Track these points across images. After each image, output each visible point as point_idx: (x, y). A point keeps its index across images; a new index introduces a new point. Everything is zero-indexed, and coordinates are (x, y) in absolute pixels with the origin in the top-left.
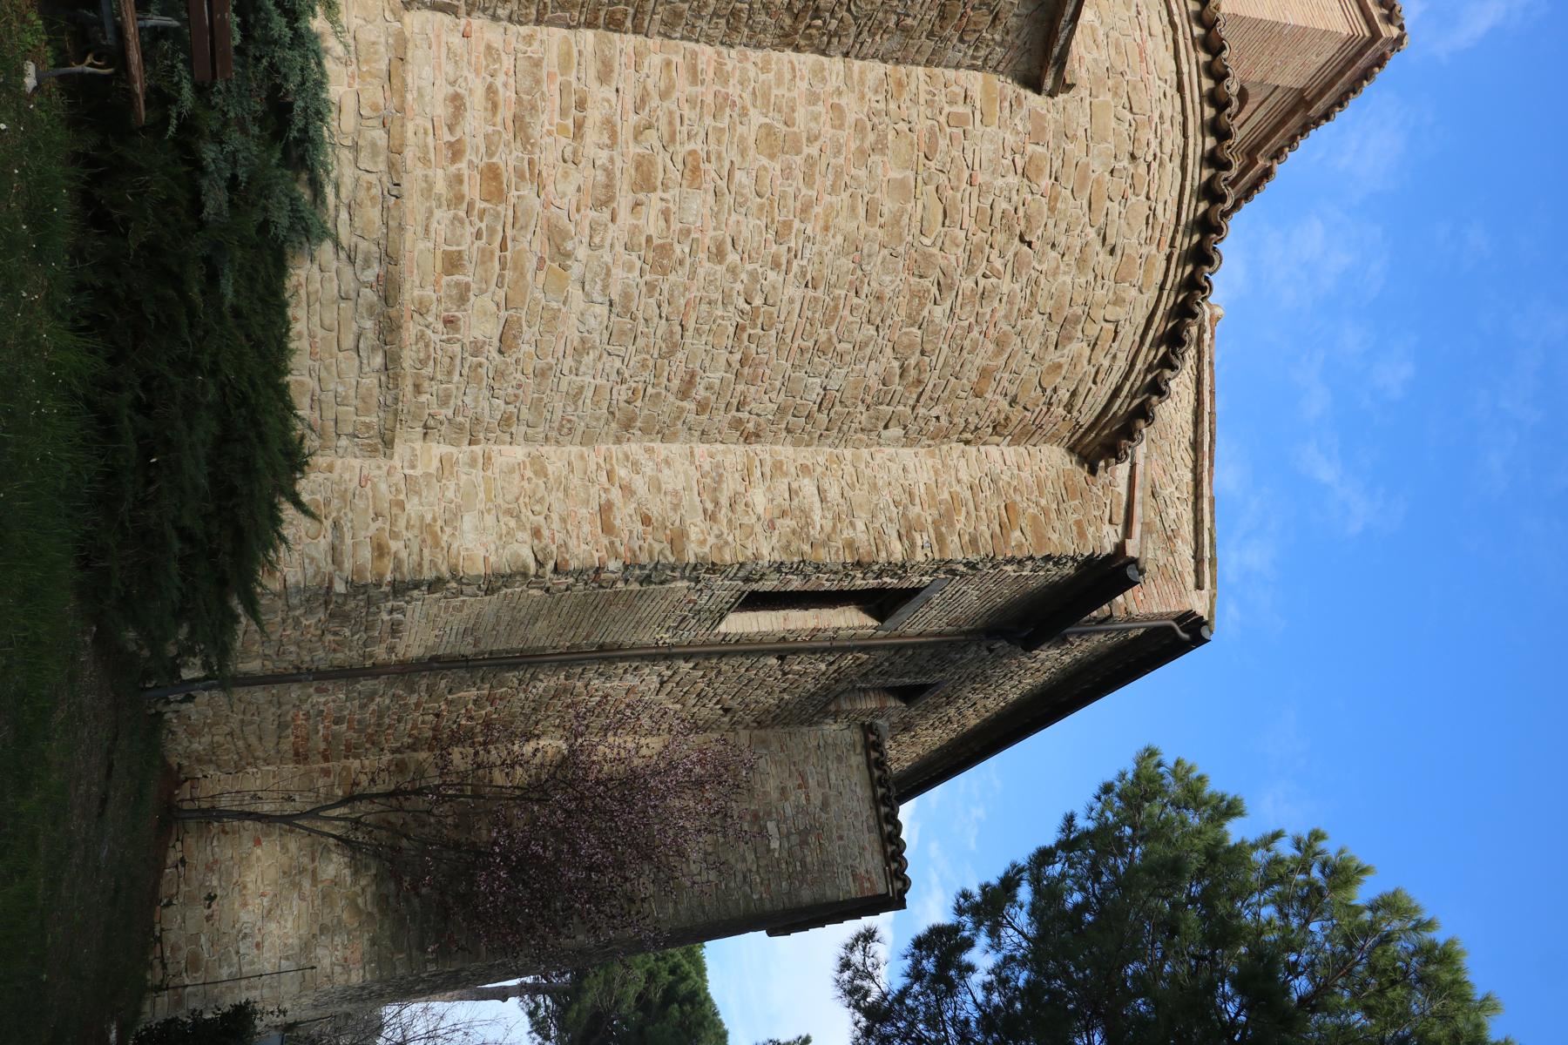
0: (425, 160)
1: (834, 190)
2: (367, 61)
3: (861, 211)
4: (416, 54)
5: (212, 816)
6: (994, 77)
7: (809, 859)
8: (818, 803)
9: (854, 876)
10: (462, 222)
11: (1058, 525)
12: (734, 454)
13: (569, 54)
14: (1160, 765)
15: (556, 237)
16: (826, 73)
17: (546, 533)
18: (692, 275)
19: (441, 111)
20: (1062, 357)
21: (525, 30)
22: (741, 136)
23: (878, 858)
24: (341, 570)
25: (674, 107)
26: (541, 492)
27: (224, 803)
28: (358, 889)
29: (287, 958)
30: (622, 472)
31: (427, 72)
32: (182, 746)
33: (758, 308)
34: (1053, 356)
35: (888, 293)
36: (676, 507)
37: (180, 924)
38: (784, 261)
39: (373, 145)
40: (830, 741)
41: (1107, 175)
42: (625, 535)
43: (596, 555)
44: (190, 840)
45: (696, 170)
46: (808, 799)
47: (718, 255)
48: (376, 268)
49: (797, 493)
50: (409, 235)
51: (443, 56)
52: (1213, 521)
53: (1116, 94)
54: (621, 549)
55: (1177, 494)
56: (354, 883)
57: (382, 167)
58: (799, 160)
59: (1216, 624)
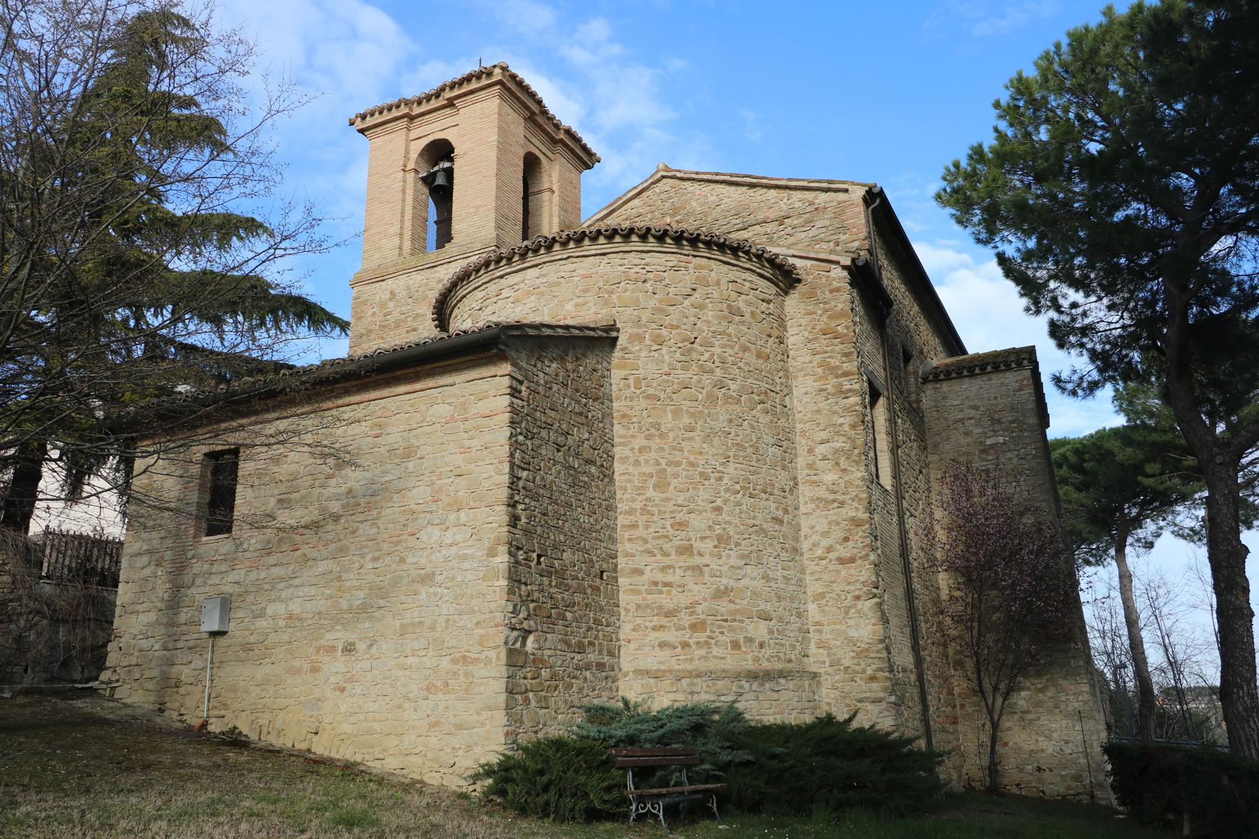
0: (691, 660)
1: (681, 450)
3: (690, 435)
4: (642, 665)
5: (994, 768)
6: (613, 363)
9: (1020, 390)
11: (833, 304)
12: (805, 491)
13: (632, 590)
14: (945, 190)
15: (720, 594)
17: (857, 593)
18: (729, 523)
19: (667, 652)
20: (746, 310)
21: (623, 613)
23: (1008, 374)
27: (986, 762)
30: (819, 552)
31: (650, 660)
32: (957, 786)
34: (748, 317)
35: (727, 416)
36: (838, 523)
37: (1055, 786)
39: (690, 685)
42: (855, 551)
44: (1006, 781)
45: (680, 524)
46: (971, 419)
47: (718, 509)
48: (743, 683)
56: (1029, 689)
59: (871, 182)
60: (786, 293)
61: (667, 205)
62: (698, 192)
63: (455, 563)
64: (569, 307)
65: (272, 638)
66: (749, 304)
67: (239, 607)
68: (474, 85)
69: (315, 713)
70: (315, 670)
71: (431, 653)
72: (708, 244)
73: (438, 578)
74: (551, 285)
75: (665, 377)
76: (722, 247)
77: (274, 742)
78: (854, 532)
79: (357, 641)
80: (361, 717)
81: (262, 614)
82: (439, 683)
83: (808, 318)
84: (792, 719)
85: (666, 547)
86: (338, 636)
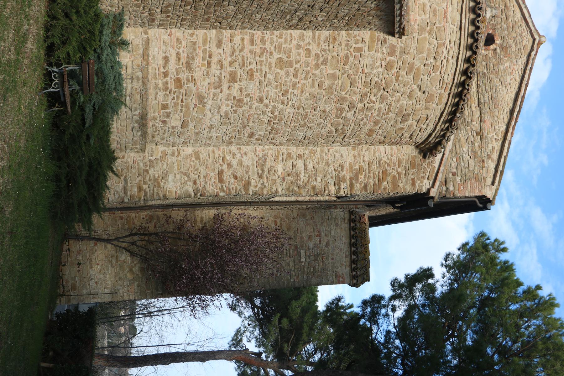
0: (155, 78)
1: (305, 78)
2: (135, 51)
3: (316, 85)
4: (153, 44)
7: (317, 267)
8: (325, 243)
9: (336, 276)
10: (168, 95)
11: (404, 180)
12: (271, 151)
13: (206, 39)
14: (488, 239)
15: (201, 98)
16: (305, 37)
17: (198, 182)
18: (251, 107)
19: (161, 62)
20: (405, 125)
21: (190, 32)
22: (270, 63)
23: (348, 269)
24: (127, 196)
25: (244, 54)
26: (197, 166)
28: (133, 264)
29: (107, 289)
30: (228, 158)
31: (156, 50)
33: (276, 116)
35: (327, 110)
36: (247, 172)
38: (286, 102)
39: (138, 77)
40: (334, 216)
41: (422, 66)
42: (227, 183)
43: (216, 191)
45: (252, 75)
46: (320, 241)
47: (261, 100)
48: (139, 111)
49: (295, 166)
50: (150, 100)
51: (162, 43)
52: (507, 153)
53: (430, 33)
54: (225, 189)
55: (495, 137)
56: (132, 262)
57: (141, 83)
58: (292, 69)
60: (417, 147)
61: (511, 42)
62: (516, 67)
66: (410, 127)
72: (457, 105)
75: (361, 69)
76: (453, 114)
78: (240, 183)
83: (396, 161)
84: (114, 137)
85: (236, 65)
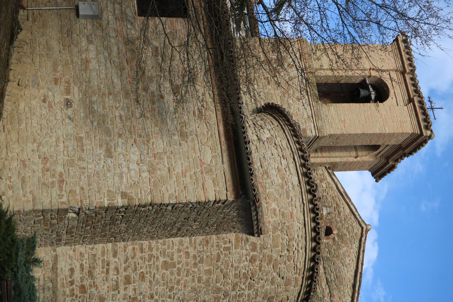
0: (63, 286)
1: (187, 276)
3: (196, 280)
4: (60, 259)
13: (104, 251)
19: (67, 273)
21: (91, 246)
31: (63, 263)
61: (345, 231)
62: (352, 251)
63: (118, 171)
64: (274, 205)
65: (75, 50)
67: (94, 25)
68: (421, 117)
69: (30, 84)
70: (56, 81)
71: (66, 158)
72: (310, 286)
73: (109, 160)
74: (287, 192)
77: (13, 57)
79: (72, 109)
80: (29, 115)
81: (90, 42)
82: (48, 165)
85: (130, 270)
86: (76, 95)
